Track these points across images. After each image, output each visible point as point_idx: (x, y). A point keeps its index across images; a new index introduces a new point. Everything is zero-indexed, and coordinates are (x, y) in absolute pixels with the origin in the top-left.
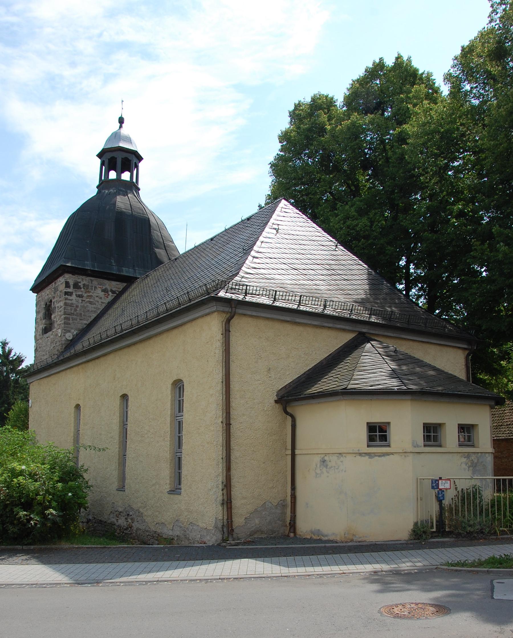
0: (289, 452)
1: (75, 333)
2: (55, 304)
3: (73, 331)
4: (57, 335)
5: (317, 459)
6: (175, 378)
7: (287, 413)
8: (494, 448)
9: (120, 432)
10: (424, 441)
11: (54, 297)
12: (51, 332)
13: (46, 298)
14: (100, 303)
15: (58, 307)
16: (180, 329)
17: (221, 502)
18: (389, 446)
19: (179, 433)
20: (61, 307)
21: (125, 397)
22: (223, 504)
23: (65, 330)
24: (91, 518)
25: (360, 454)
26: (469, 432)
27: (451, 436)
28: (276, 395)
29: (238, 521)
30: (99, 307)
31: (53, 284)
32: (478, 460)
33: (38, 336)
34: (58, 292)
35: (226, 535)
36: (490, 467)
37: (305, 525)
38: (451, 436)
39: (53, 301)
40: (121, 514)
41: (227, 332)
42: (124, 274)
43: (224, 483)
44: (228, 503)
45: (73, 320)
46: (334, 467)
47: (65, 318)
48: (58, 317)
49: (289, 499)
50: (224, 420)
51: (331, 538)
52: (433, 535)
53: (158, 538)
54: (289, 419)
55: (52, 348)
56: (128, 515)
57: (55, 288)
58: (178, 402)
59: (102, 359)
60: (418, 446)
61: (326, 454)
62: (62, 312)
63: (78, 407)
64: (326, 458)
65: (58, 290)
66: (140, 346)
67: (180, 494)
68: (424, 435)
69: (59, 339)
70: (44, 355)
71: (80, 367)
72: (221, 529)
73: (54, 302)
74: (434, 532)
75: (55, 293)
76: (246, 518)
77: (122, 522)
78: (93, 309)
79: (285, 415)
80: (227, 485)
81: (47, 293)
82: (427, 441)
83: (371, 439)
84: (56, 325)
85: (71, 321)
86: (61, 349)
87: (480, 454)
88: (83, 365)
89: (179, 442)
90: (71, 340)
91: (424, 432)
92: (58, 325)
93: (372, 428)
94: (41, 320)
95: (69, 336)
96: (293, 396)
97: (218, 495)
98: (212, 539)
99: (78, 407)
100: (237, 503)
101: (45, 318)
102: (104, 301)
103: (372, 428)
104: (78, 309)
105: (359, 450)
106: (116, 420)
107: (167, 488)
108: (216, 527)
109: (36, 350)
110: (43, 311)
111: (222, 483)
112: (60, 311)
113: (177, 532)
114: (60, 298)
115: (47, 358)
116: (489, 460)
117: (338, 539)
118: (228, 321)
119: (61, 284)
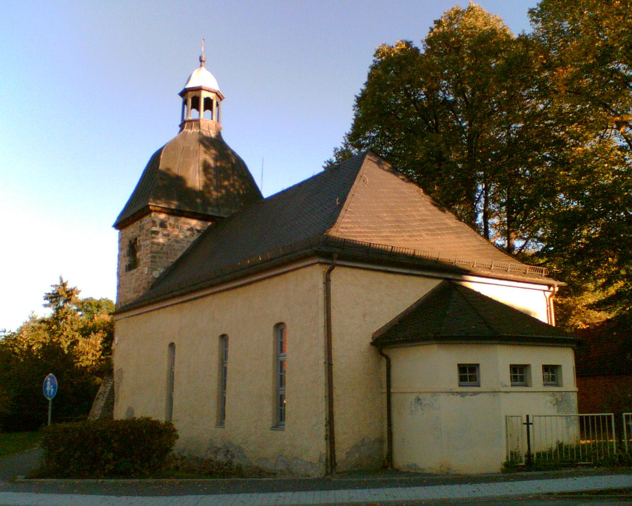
0: (385, 390)
1: (162, 271)
2: (141, 241)
3: (159, 269)
4: (142, 273)
5: (413, 397)
6: (278, 321)
7: (382, 354)
8: (577, 386)
9: (219, 371)
10: (511, 381)
11: (139, 236)
12: (136, 270)
13: (131, 235)
14: (186, 242)
15: (144, 246)
16: (282, 277)
17: (325, 437)
18: (479, 386)
19: (281, 372)
20: (148, 245)
21: (224, 338)
22: (326, 439)
23: (152, 268)
24: (186, 455)
25: (453, 393)
26: (553, 372)
27: (537, 375)
28: (372, 338)
29: (340, 455)
30: (185, 245)
31: (139, 222)
32: (562, 398)
33: (121, 273)
34: (144, 231)
35: (329, 470)
36: (575, 404)
37: (401, 459)
38: (537, 375)
39: (138, 239)
40: (220, 450)
41: (327, 282)
42: (210, 213)
43: (327, 420)
44: (331, 437)
45: (159, 258)
46: (429, 405)
47: (152, 257)
48: (143, 255)
49: (386, 436)
50: (327, 361)
51: (428, 471)
52: (521, 469)
53: (260, 472)
54: (384, 360)
55: (137, 285)
56: (228, 451)
57: (140, 226)
58: (279, 343)
59: (199, 301)
60: (506, 386)
61: (420, 393)
62: (149, 251)
63: (172, 345)
64: (421, 396)
65: (144, 229)
66: (240, 290)
67: (283, 430)
68: (511, 376)
69: (146, 276)
70: (127, 292)
71: (175, 307)
72: (325, 464)
73: (139, 240)
74: (522, 466)
75: (140, 231)
76: (347, 453)
77: (220, 458)
78: (179, 248)
79: (380, 356)
80: (330, 422)
81: (131, 231)
82: (514, 381)
83: (462, 379)
84: (141, 263)
85: (157, 260)
86: (148, 287)
87: (564, 393)
88: (179, 306)
89: (281, 381)
90: (158, 279)
91: (511, 373)
92: (144, 263)
93: (462, 368)
94: (124, 257)
95: (156, 274)
96: (389, 340)
97: (322, 431)
98: (318, 472)
99: (172, 345)
100: (339, 438)
101: (129, 255)
102: (190, 240)
103: (462, 368)
104: (164, 248)
105: (451, 390)
106: (214, 360)
107: (270, 424)
108: (320, 460)
109: (119, 287)
110: (128, 248)
111: (326, 419)
112: (147, 249)
113: (280, 467)
114: (146, 236)
115: (132, 296)
116: (574, 398)
117: (434, 472)
118: (329, 272)
119: (148, 223)
